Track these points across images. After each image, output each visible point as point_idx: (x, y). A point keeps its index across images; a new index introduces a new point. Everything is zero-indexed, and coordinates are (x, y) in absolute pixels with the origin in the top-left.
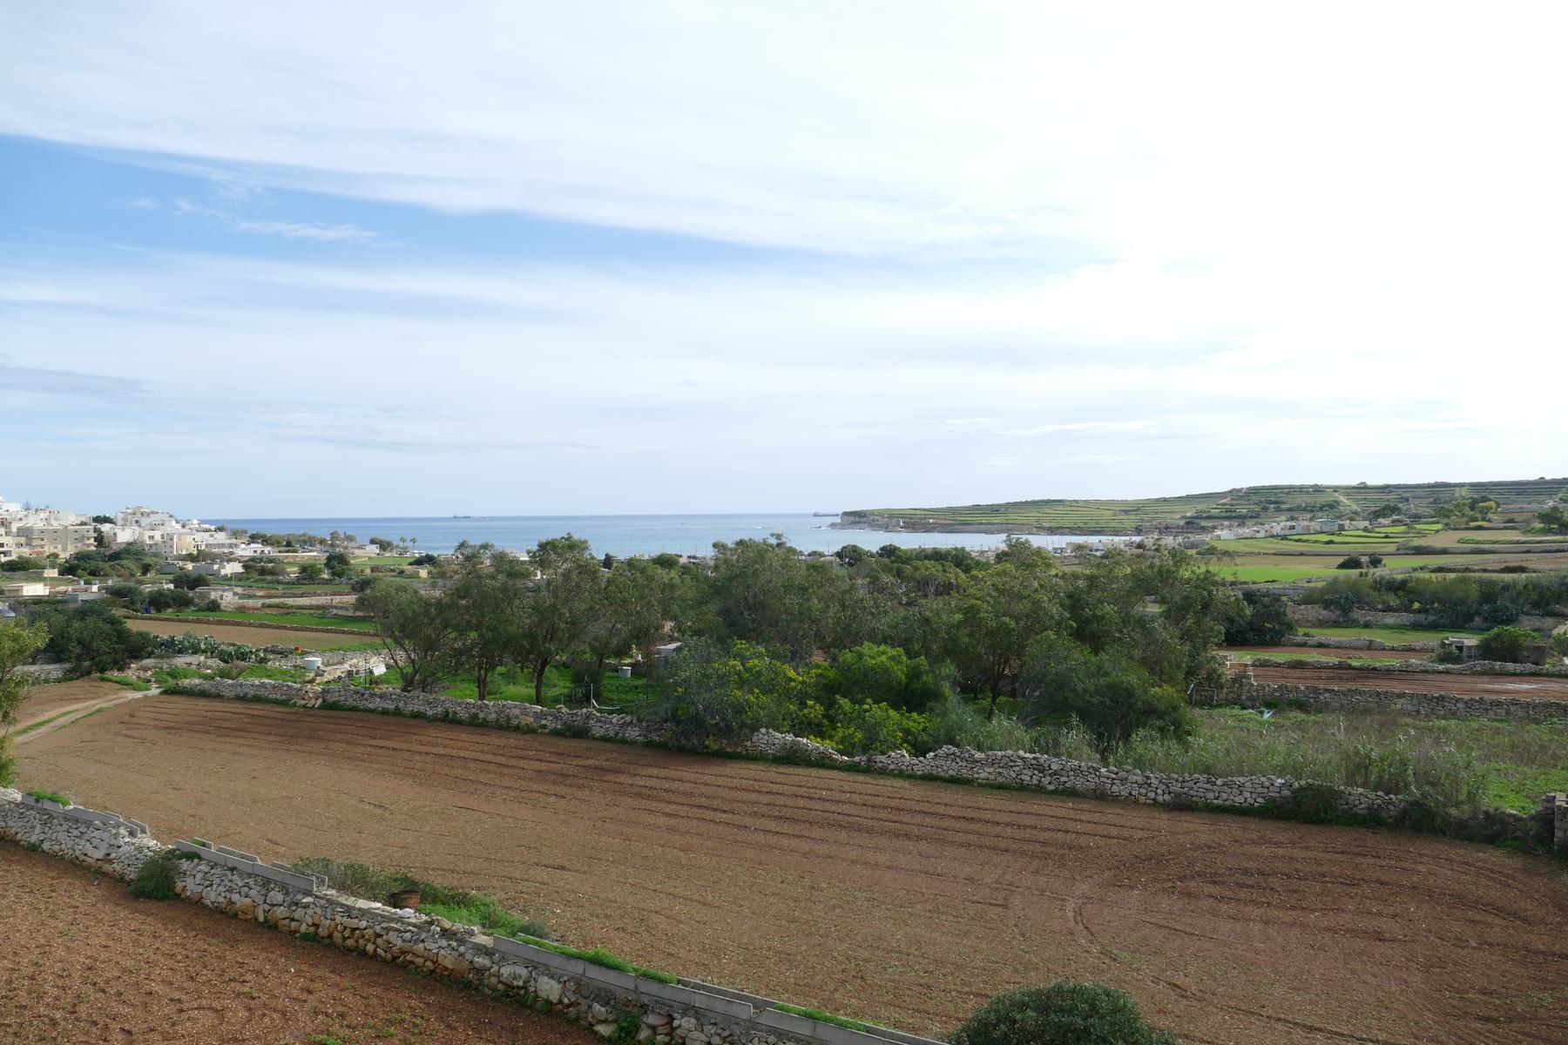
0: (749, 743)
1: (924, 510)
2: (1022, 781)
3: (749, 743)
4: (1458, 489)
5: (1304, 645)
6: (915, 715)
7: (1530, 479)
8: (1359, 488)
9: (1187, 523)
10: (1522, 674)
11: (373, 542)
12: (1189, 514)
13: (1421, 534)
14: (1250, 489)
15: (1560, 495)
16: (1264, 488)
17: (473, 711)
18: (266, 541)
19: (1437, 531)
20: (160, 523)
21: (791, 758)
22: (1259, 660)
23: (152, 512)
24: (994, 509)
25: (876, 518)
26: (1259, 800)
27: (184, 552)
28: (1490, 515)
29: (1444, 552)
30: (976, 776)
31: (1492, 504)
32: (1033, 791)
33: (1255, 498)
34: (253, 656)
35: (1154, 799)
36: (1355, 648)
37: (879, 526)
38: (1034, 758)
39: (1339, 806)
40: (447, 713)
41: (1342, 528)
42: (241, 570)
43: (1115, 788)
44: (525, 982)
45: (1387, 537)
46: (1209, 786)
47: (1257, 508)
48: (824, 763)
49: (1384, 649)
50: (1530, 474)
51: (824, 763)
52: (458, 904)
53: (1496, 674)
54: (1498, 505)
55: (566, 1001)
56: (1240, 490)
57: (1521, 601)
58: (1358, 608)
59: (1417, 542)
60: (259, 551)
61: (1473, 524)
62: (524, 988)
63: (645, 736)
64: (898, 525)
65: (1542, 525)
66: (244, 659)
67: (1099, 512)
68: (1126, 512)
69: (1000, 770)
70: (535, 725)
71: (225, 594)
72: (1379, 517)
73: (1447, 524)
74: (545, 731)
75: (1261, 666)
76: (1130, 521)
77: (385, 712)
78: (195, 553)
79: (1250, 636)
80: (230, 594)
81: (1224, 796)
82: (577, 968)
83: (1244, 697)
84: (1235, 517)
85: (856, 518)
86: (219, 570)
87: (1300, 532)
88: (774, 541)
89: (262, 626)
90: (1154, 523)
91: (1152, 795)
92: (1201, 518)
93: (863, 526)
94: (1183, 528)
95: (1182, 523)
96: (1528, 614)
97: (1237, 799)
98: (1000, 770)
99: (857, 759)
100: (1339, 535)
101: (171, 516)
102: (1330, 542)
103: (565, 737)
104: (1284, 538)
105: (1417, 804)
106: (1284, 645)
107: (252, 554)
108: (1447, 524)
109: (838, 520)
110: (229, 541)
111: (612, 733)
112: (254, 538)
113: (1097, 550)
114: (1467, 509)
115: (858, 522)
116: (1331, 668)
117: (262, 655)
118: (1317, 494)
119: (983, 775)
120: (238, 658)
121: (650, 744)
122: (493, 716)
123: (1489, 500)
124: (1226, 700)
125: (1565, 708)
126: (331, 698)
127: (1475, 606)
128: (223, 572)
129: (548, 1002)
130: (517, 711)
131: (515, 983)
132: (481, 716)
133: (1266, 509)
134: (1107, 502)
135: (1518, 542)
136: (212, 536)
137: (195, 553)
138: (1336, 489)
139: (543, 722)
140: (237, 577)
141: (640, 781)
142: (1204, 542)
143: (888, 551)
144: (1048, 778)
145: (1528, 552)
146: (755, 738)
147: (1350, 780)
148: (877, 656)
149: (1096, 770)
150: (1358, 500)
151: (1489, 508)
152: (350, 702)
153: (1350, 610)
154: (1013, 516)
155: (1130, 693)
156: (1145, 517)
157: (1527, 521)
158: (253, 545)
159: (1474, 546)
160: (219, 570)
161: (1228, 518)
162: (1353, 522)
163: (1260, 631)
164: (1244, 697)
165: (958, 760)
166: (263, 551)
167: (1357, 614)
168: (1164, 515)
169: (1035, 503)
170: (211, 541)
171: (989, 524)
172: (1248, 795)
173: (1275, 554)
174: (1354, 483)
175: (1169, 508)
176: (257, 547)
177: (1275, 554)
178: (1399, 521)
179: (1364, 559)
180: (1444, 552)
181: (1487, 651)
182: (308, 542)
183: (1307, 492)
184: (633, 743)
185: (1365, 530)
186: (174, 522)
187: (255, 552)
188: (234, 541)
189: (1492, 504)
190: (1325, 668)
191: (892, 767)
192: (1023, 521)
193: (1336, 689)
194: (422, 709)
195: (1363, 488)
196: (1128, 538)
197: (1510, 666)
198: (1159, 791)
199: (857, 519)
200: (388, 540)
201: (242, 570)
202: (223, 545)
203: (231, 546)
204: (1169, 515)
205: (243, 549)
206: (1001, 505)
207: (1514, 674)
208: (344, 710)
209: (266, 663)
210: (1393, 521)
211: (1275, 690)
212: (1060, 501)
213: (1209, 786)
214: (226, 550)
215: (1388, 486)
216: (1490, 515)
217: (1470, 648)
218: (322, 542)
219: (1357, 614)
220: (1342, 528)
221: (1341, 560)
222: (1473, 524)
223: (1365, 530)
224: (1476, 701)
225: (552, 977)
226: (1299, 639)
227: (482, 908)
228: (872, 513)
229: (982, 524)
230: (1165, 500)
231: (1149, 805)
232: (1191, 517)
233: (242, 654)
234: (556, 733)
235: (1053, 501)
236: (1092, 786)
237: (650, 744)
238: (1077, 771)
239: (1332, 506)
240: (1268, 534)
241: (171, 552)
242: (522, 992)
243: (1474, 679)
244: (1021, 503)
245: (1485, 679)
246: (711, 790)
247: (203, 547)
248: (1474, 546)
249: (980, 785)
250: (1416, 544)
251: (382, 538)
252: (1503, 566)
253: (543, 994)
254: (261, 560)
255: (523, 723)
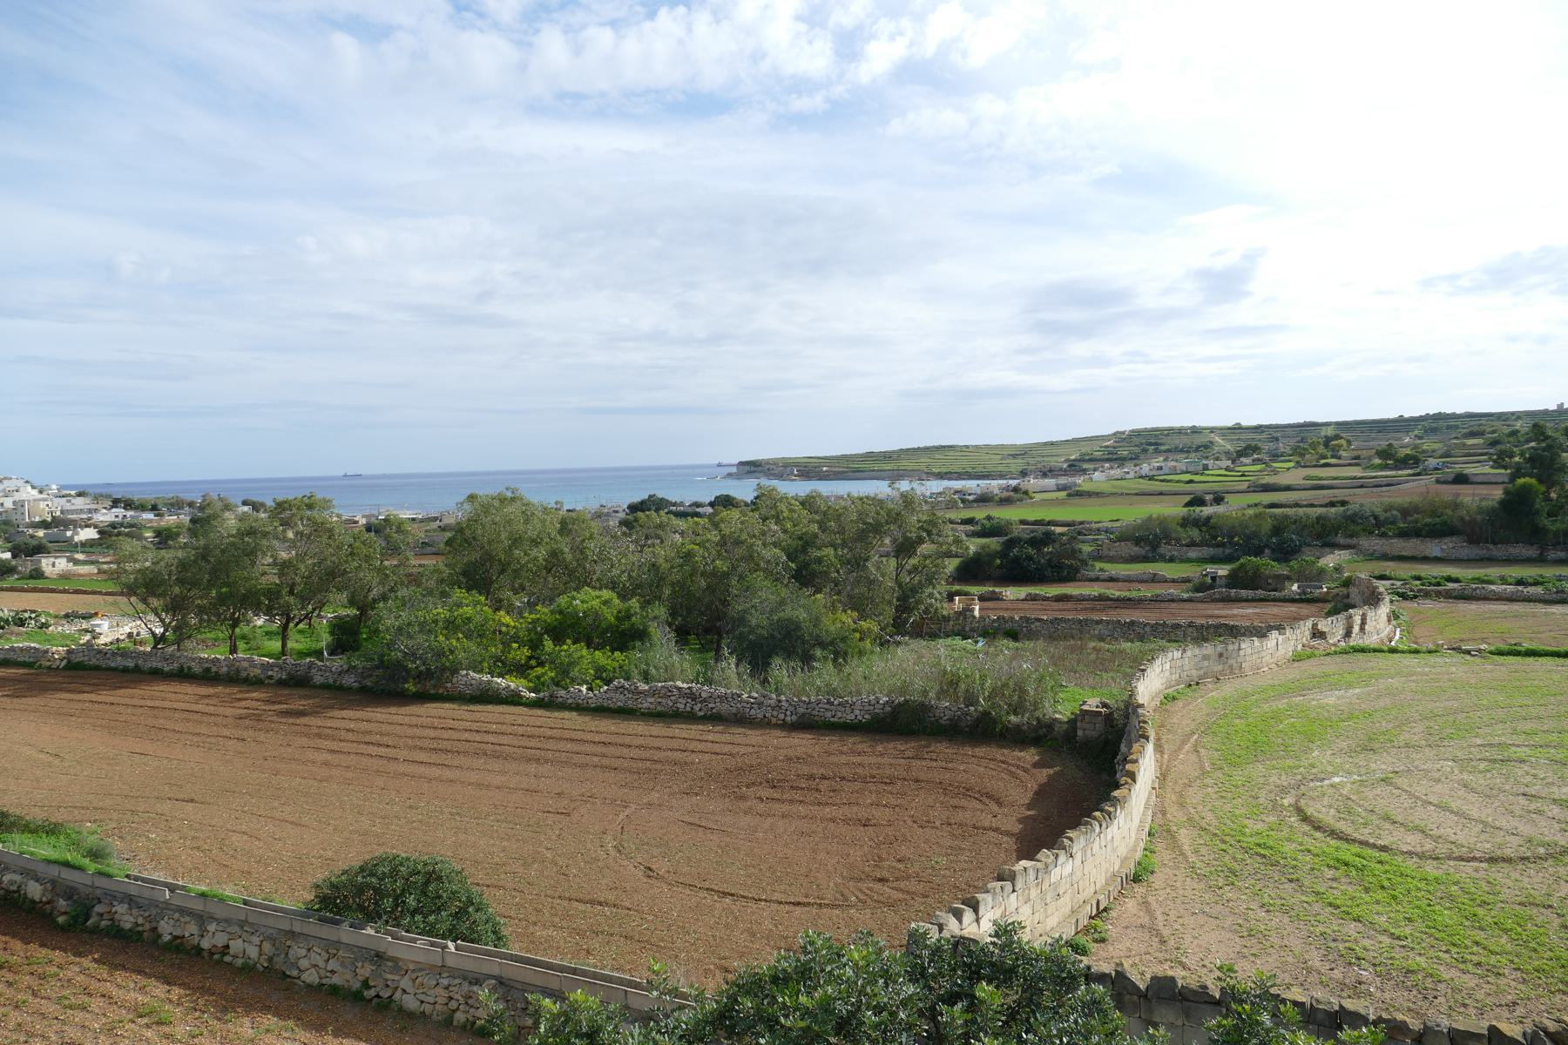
0: (449, 685)
1: (819, 458)
2: (678, 708)
3: (449, 685)
4: (1324, 428)
5: (1097, 579)
6: (617, 654)
7: (1391, 417)
8: (1235, 429)
9: (1069, 466)
10: (1253, 600)
11: (245, 503)
12: (1073, 457)
13: (1275, 472)
14: (1133, 431)
15: (1416, 432)
16: (1146, 430)
17: (206, 665)
18: (128, 505)
19: (1288, 469)
20: (15, 488)
21: (487, 697)
22: (1030, 594)
23: (5, 478)
24: (887, 456)
25: (771, 467)
26: (866, 716)
27: (37, 519)
28: (1341, 452)
29: (1288, 488)
30: (640, 706)
31: (1343, 442)
32: (685, 718)
33: (1136, 440)
34: (33, 622)
35: (783, 720)
36: (1141, 581)
37: (774, 475)
38: (689, 688)
39: (928, 719)
40: (181, 669)
41: (1206, 468)
42: (97, 536)
43: (753, 711)
44: (19, 887)
45: (1242, 476)
46: (828, 707)
47: (1137, 450)
48: (514, 699)
49: (1166, 581)
50: (1390, 413)
51: (514, 699)
52: (47, 833)
53: (1232, 601)
54: (1349, 442)
55: (44, 899)
56: (1123, 433)
57: (1306, 533)
58: (1165, 544)
59: (1267, 480)
60: (121, 517)
61: (1323, 461)
62: (18, 891)
63: (359, 682)
64: (792, 473)
65: (1380, 461)
66: (22, 625)
67: (988, 457)
68: (1014, 456)
69: (660, 700)
70: (262, 676)
71: (57, 561)
72: (1241, 456)
73: (1298, 462)
74: (272, 682)
75: (1032, 600)
76: (1016, 465)
77: (126, 670)
78: (49, 519)
79: (1048, 572)
80: (64, 561)
81: (839, 714)
82: (54, 871)
83: (967, 629)
84: (1116, 459)
85: (751, 468)
86: (72, 537)
87: (1167, 472)
88: (509, 494)
89: (76, 592)
90: (1039, 466)
91: (782, 716)
92: (1084, 461)
93: (758, 475)
94: (1065, 470)
95: (1065, 466)
96: (1309, 545)
97: (848, 717)
98: (660, 700)
99: (542, 695)
100: (1202, 474)
101: (27, 482)
102: (1191, 482)
103: (289, 686)
104: (1151, 478)
105: (986, 714)
106: (1080, 581)
107: (113, 519)
108: (1298, 462)
109: (734, 470)
110: (88, 507)
111: (331, 681)
112: (116, 503)
113: (970, 495)
114: (1322, 447)
115: (754, 472)
116: (1092, 600)
117: (43, 621)
118: (1195, 436)
119: (645, 705)
120: (15, 624)
121: (363, 690)
122: (225, 669)
123: (1342, 438)
124: (953, 631)
125: (3, 590)
126: (76, 659)
127: (1264, 539)
128: (76, 539)
129: (33, 901)
130: (246, 664)
131: (11, 888)
132: (214, 669)
133: (1145, 451)
134: (997, 447)
135: (1355, 478)
136: (69, 501)
137: (49, 519)
138: (1212, 430)
139: (270, 673)
140: (87, 545)
141: (329, 723)
142: (1075, 484)
143: (808, 503)
144: (699, 705)
145: (1362, 487)
146: (455, 680)
147: (942, 693)
148: (589, 600)
149: (739, 696)
150: (1232, 440)
151: (1340, 446)
152: (94, 661)
153: (1158, 545)
154: (904, 463)
155: (798, 627)
156: (1031, 460)
157: (1370, 458)
158: (114, 510)
159: (1315, 482)
160: (72, 537)
161: (1108, 460)
162: (1217, 462)
163: (1060, 567)
164: (967, 629)
165: (626, 692)
166: (125, 516)
167: (1164, 549)
168: (1050, 459)
169: (927, 449)
170: (68, 507)
171: (881, 471)
172: (857, 712)
173: (1136, 494)
174: (1230, 424)
175: (1055, 451)
176: (120, 511)
177: (1136, 494)
178: (1258, 460)
179: (1208, 498)
180: (1288, 488)
181: (1234, 580)
182: (176, 505)
183: (1186, 434)
184: (349, 689)
185: (1227, 469)
186: (29, 488)
187: (117, 516)
188: (94, 506)
189: (1343, 442)
190: (1087, 600)
191: (570, 701)
192: (915, 468)
193: (1045, 618)
194: (159, 665)
195: (1237, 428)
196: (1005, 482)
197: (1244, 593)
198: (788, 713)
199: (752, 468)
200: (261, 501)
201: (97, 536)
202: (81, 511)
203: (90, 511)
204: (1055, 458)
205: (104, 514)
206: (894, 451)
207: (1247, 600)
208: (86, 669)
209: (47, 628)
210: (1254, 460)
211: (994, 621)
212: (951, 447)
213: (828, 707)
214: (84, 516)
215: (1261, 426)
216: (1341, 452)
217: (1221, 577)
218: (191, 504)
219: (1164, 549)
220: (1206, 468)
221: (1187, 498)
222: (1323, 461)
223: (1227, 469)
224: (1161, 625)
225: (37, 881)
226: (1092, 574)
227: (73, 836)
228: (768, 462)
229: (873, 471)
230: (1052, 444)
231: (779, 725)
232: (1074, 460)
233: (20, 619)
234: (281, 683)
235: (944, 447)
236: (734, 710)
237: (363, 690)
238: (723, 698)
239: (1207, 446)
240: (1137, 475)
241: (24, 519)
242: (16, 895)
243: (1212, 606)
244: (914, 449)
245: (1220, 605)
246: (385, 728)
247: (58, 513)
248: (1315, 482)
249: (643, 714)
250: (1264, 482)
251: (255, 499)
252: (1327, 501)
253: (30, 896)
254: (122, 525)
255: (252, 675)
